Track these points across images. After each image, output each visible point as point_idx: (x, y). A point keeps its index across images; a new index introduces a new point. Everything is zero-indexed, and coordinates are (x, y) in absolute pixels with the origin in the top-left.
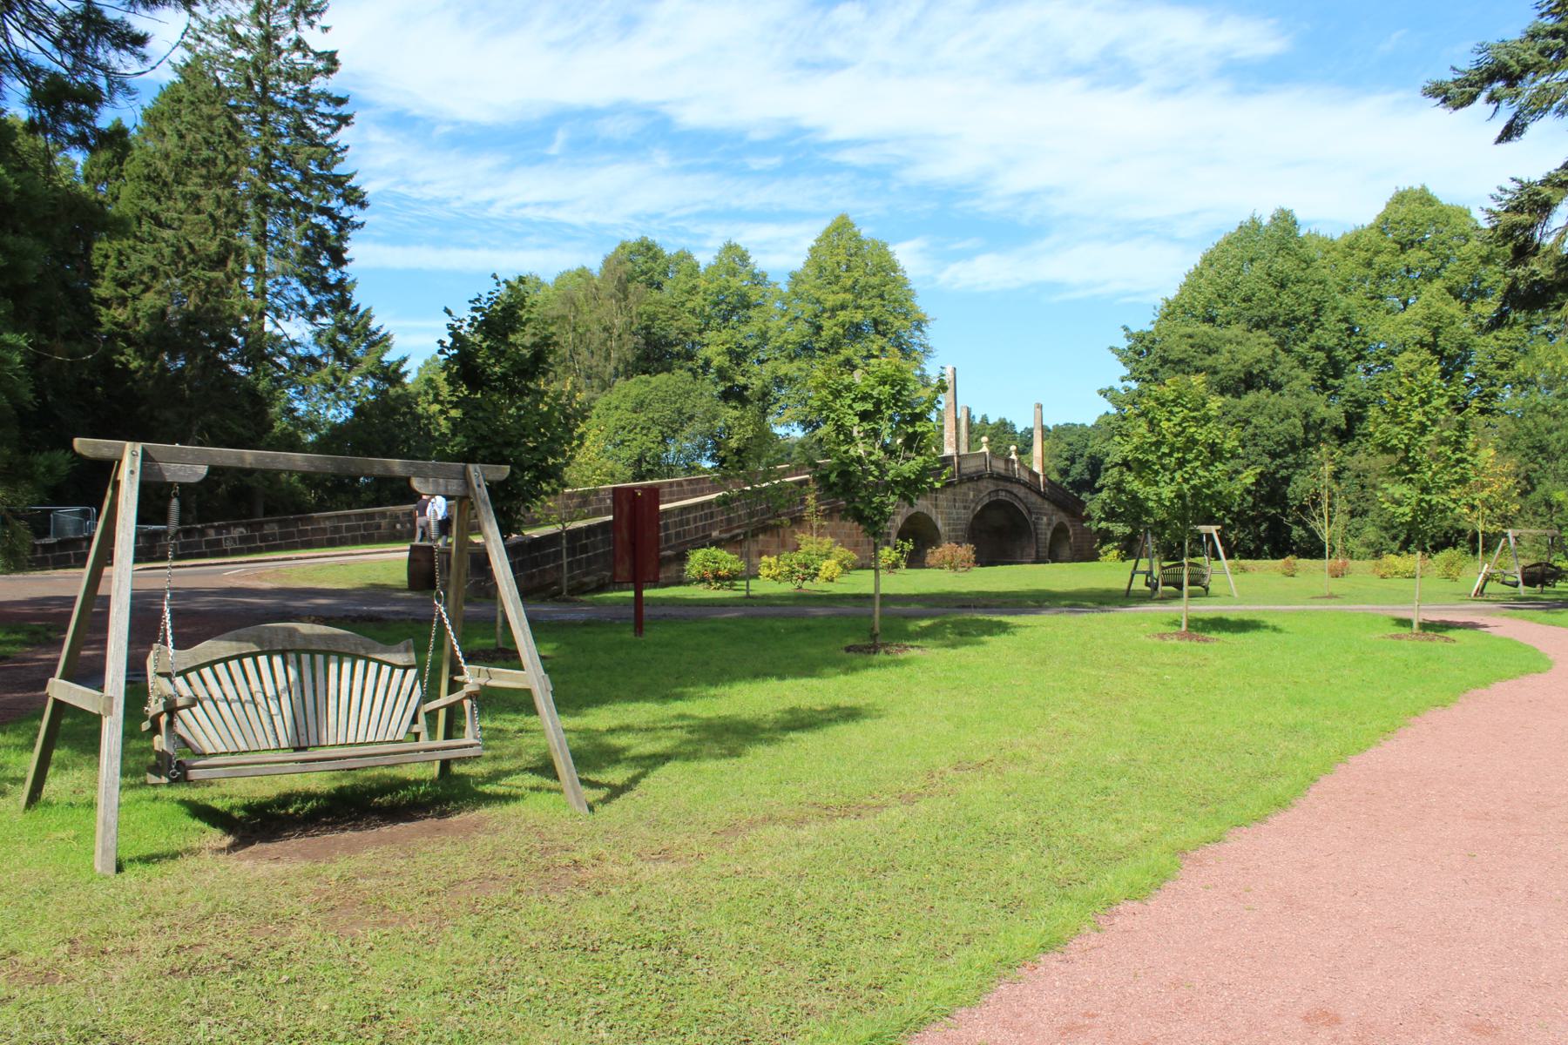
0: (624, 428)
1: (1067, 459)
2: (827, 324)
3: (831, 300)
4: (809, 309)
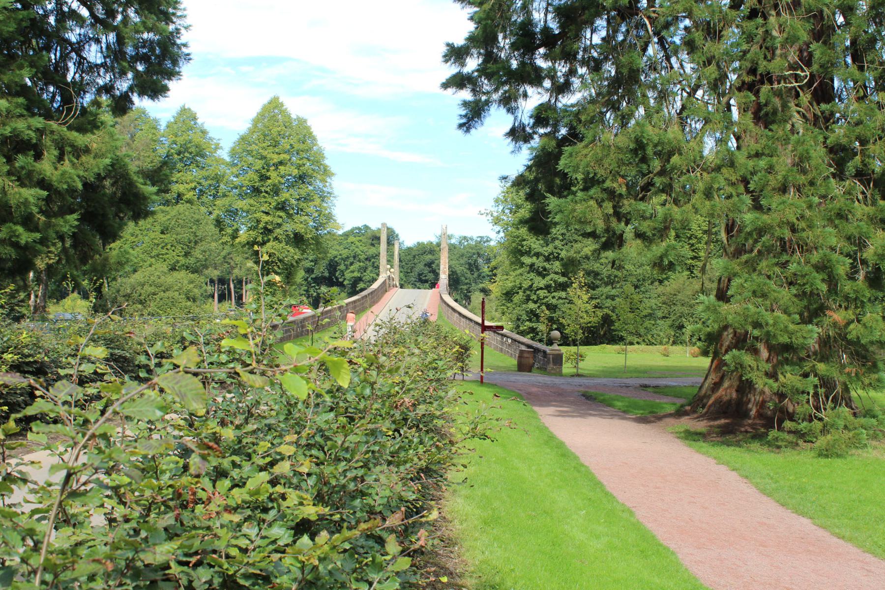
0: (158, 245)
1: (312, 261)
2: (273, 174)
3: (276, 158)
4: (259, 164)
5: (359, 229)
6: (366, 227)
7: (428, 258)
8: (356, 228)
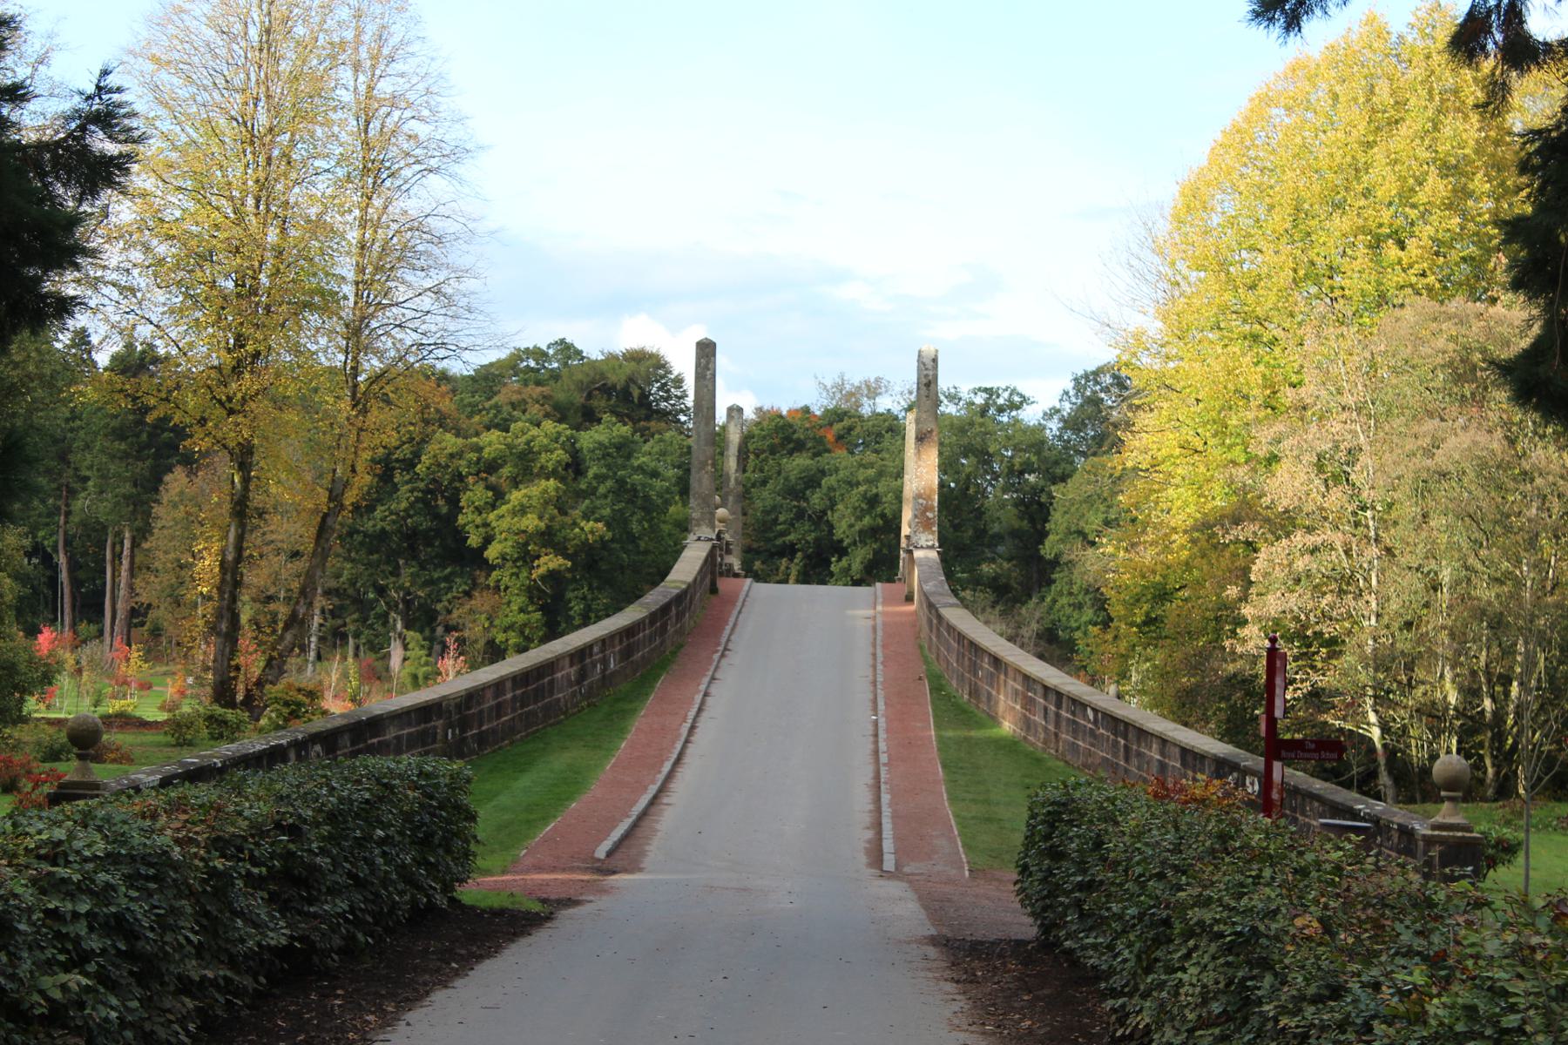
5: (539, 354)
6: (566, 349)
7: (799, 463)
8: (529, 353)
